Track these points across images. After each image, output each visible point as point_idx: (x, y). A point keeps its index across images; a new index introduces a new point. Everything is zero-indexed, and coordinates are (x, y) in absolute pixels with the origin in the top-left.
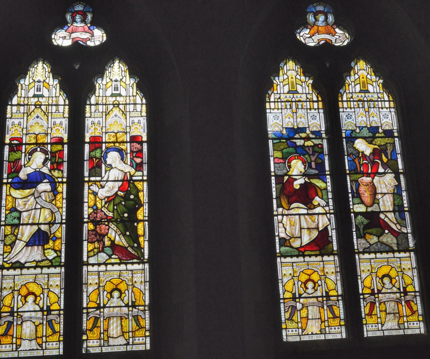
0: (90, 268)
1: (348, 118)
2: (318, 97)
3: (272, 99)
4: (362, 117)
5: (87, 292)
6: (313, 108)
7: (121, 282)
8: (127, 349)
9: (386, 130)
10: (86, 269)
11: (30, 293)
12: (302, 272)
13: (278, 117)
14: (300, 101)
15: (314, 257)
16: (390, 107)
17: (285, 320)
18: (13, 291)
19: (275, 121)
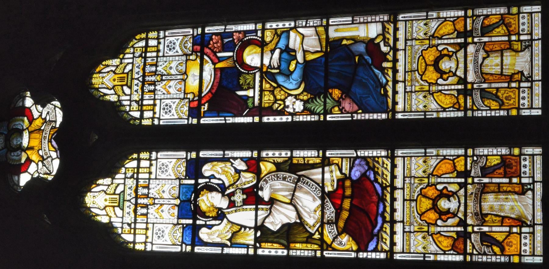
0: (398, 248)
1: (174, 48)
2: (133, 159)
3: (137, 114)
4: (170, 87)
5: (437, 112)
6: (157, 46)
7: (424, 58)
8: (539, 81)
9: (186, 171)
10: (399, 255)
11: (436, 64)
12: (422, 76)
13: (163, 165)
14: (136, 191)
15: (396, 170)
16: (150, 159)
17: (505, 255)
18: (430, 94)
19: (173, 111)
